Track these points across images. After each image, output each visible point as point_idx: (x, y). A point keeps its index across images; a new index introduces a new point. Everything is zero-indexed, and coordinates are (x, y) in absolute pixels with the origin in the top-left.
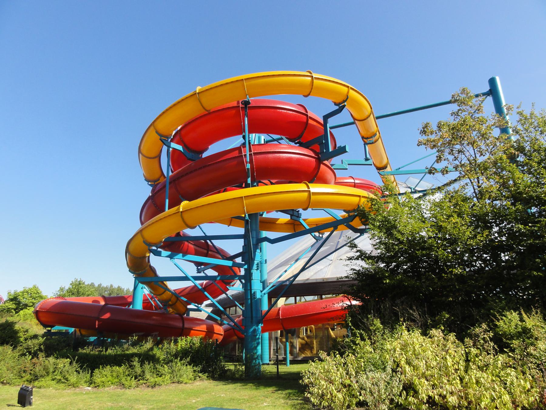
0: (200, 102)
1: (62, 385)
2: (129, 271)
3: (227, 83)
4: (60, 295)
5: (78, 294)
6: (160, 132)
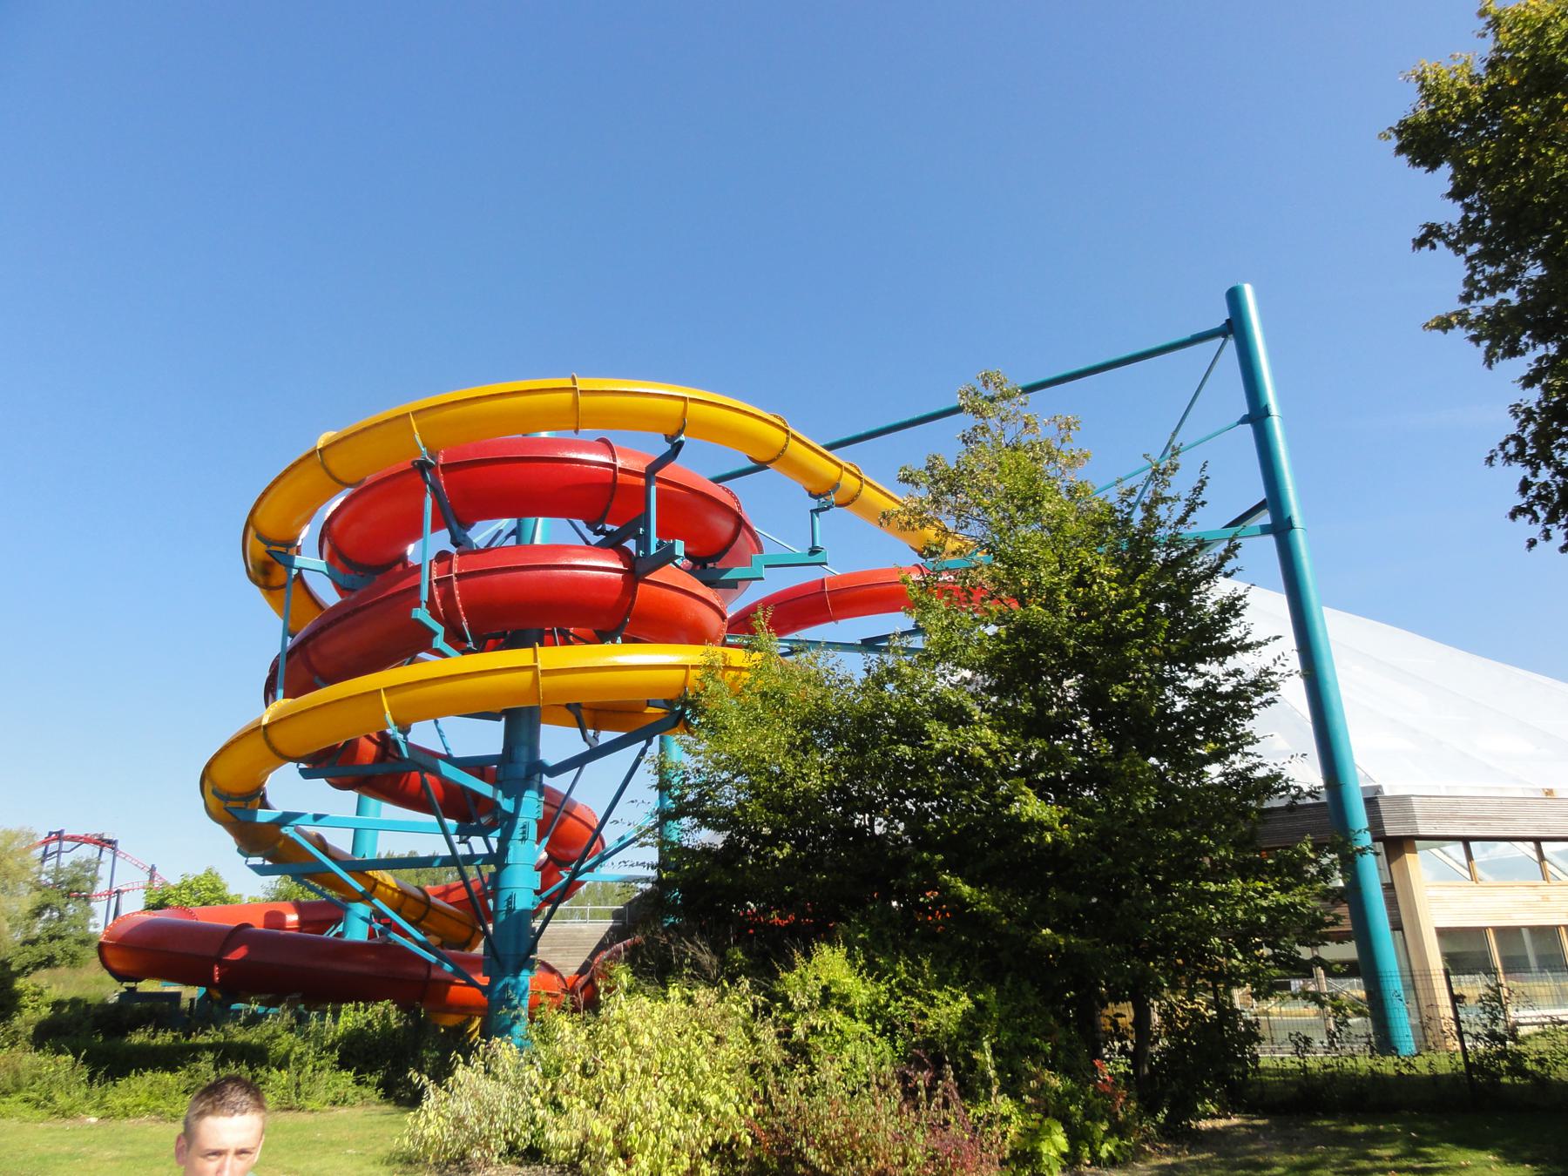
0: (326, 469)
1: (38, 1114)
2: (239, 851)
4: (280, 892)
5: (161, 905)
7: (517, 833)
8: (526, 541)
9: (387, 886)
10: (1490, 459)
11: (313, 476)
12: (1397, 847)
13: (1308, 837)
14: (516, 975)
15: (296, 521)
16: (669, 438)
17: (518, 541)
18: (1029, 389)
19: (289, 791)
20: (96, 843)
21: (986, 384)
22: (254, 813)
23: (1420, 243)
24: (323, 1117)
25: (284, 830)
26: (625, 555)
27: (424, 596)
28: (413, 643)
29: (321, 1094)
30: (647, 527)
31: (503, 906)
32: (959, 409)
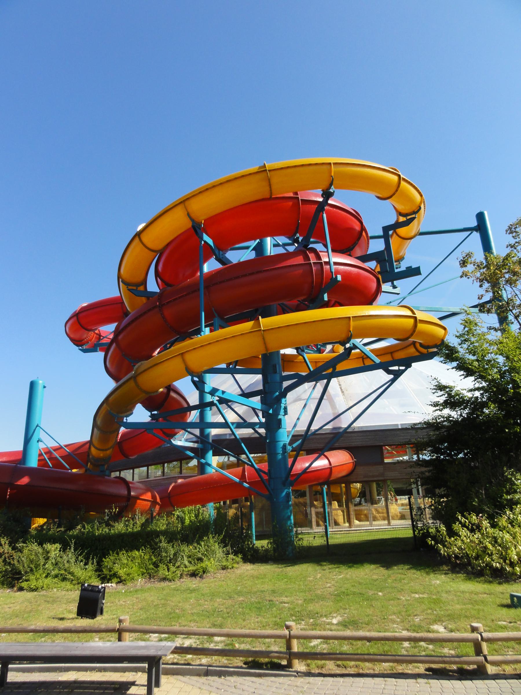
3: (310, 165)
6: (192, 215)
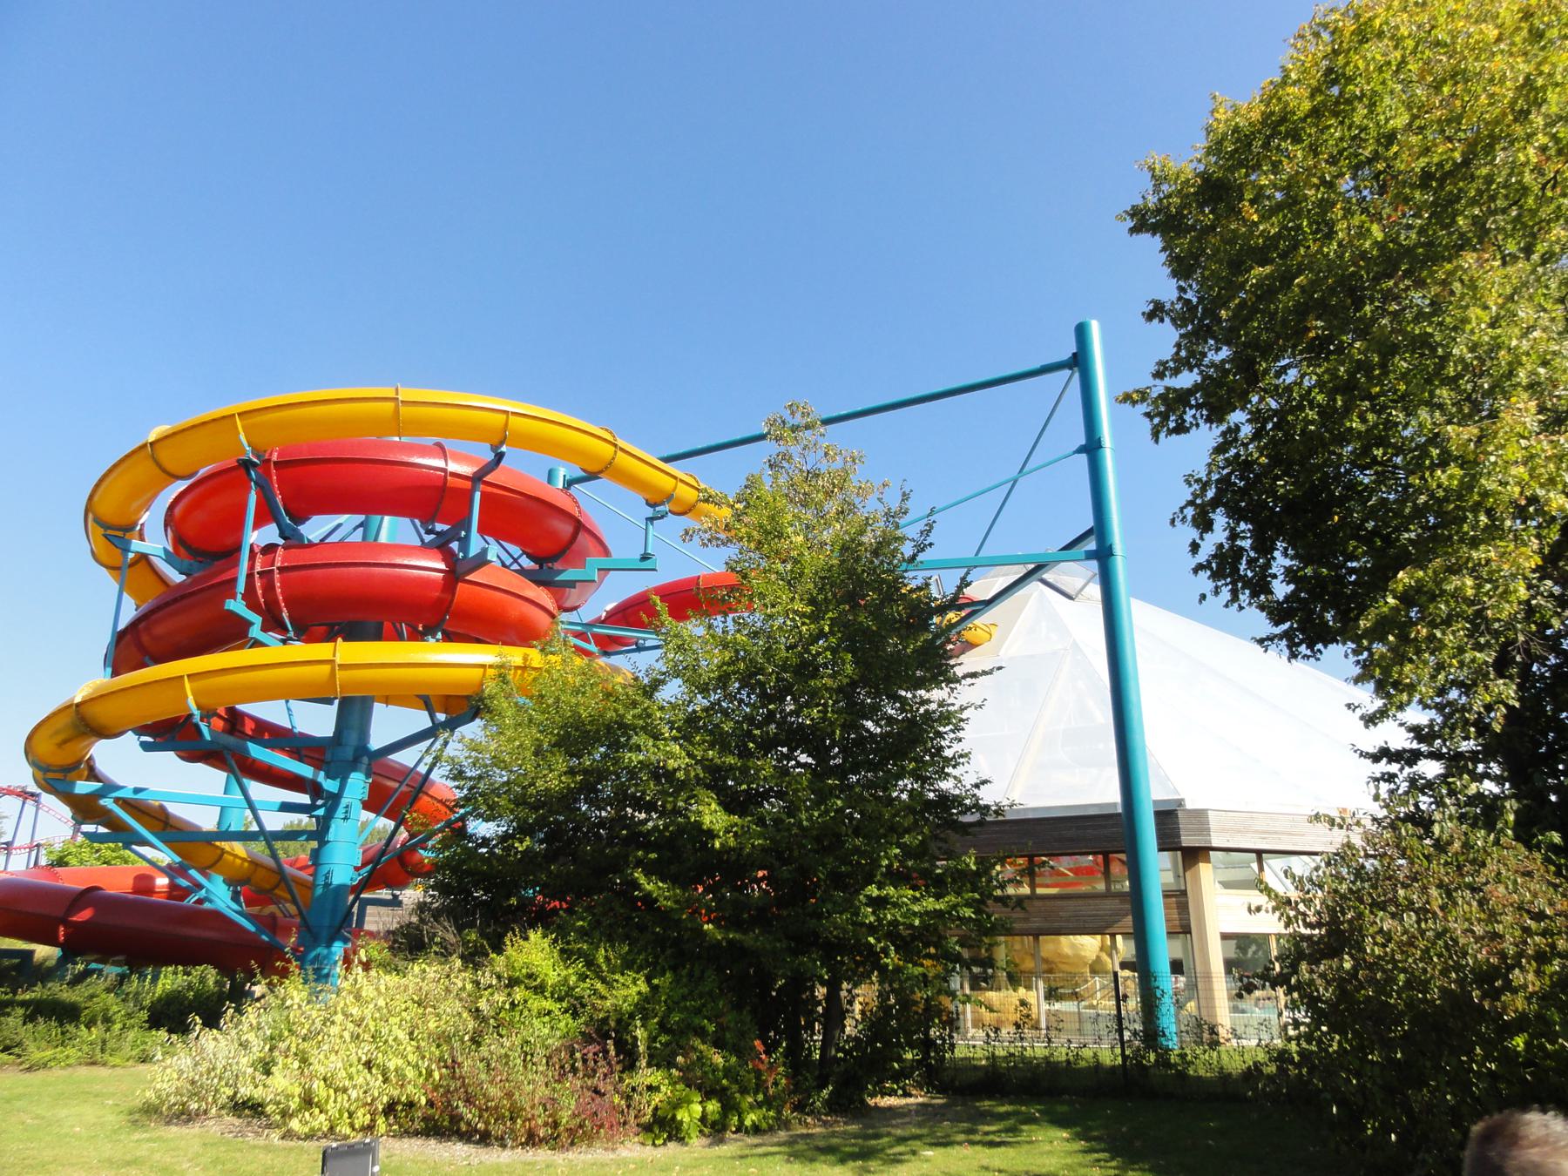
0: (158, 464)
7: (340, 812)
8: (371, 539)
9: (236, 856)
10: (1173, 522)
11: (145, 469)
12: (1194, 856)
13: (972, 851)
14: (329, 945)
15: (135, 505)
16: (494, 448)
17: (364, 537)
18: (826, 422)
19: (125, 763)
20: (18, 795)
21: (793, 413)
22: (73, 784)
23: (1150, 316)
24: (119, 1071)
25: (102, 802)
26: (448, 556)
27: (241, 587)
28: (232, 634)
29: (126, 1050)
30: (468, 531)
31: (321, 881)
32: (762, 437)
